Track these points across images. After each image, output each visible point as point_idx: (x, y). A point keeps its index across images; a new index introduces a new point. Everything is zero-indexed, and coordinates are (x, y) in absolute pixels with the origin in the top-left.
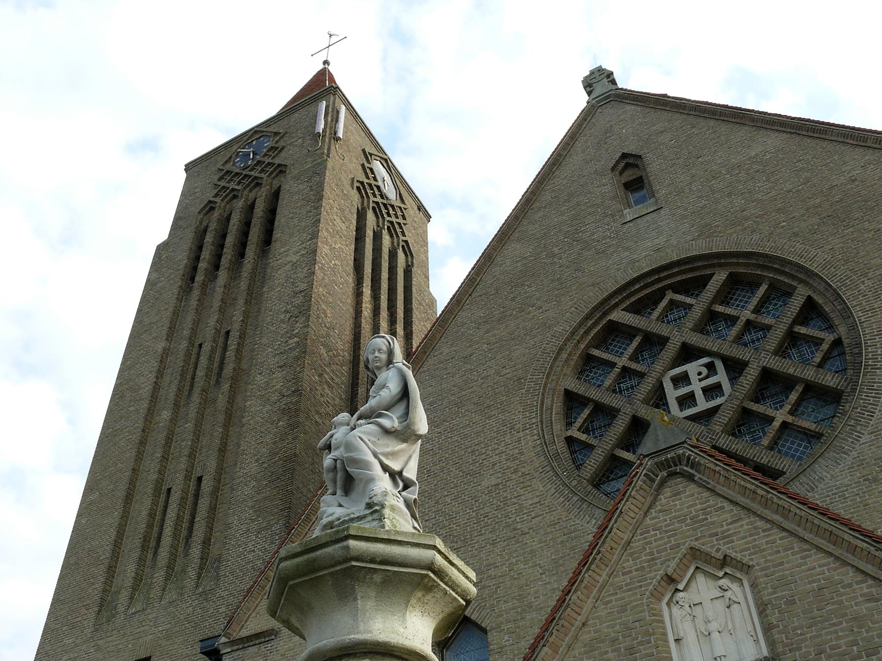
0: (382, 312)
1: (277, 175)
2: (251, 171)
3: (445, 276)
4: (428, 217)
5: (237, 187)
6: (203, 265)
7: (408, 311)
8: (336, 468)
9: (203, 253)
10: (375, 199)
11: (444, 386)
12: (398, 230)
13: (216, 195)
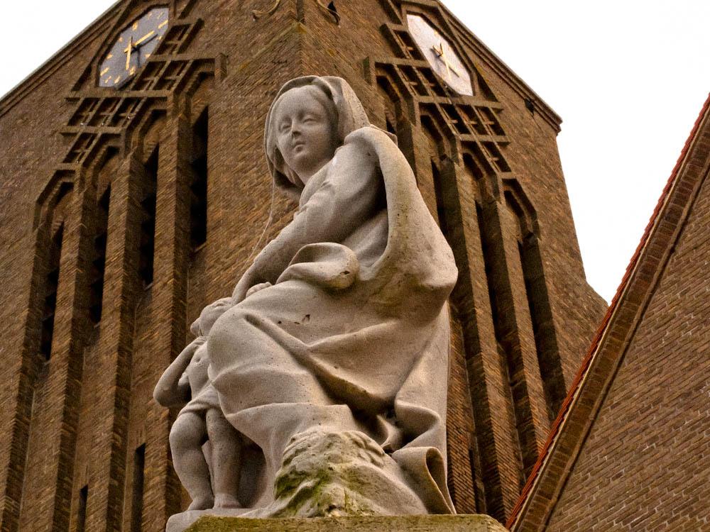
0: (484, 346)
1: (196, 86)
2: (138, 87)
3: (606, 237)
4: (554, 121)
5: (113, 130)
6: (64, 313)
7: (544, 335)
8: (204, 438)
9: (61, 287)
10: (425, 100)
11: (648, 470)
12: (490, 159)
13: (70, 158)
